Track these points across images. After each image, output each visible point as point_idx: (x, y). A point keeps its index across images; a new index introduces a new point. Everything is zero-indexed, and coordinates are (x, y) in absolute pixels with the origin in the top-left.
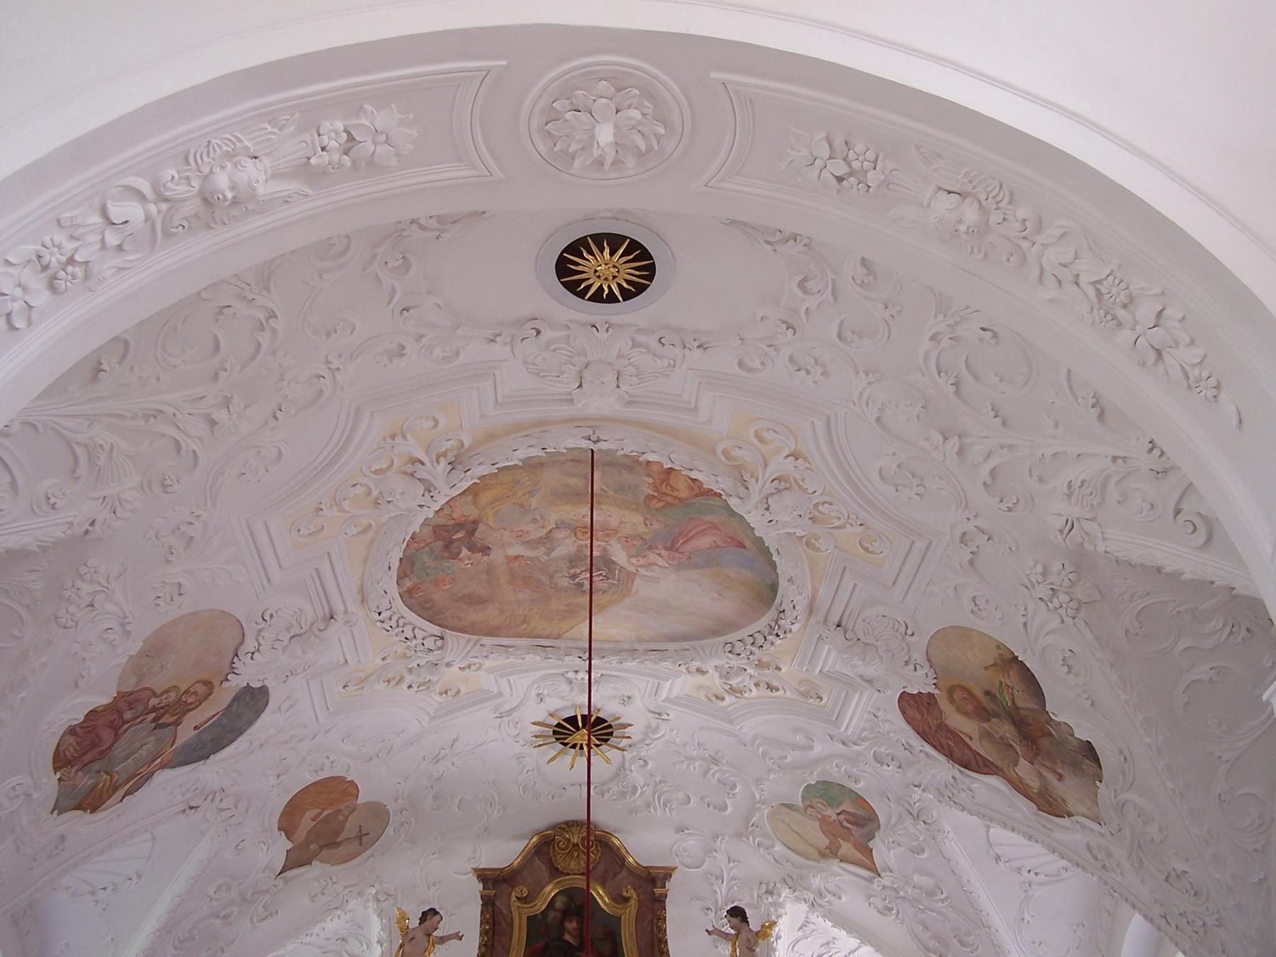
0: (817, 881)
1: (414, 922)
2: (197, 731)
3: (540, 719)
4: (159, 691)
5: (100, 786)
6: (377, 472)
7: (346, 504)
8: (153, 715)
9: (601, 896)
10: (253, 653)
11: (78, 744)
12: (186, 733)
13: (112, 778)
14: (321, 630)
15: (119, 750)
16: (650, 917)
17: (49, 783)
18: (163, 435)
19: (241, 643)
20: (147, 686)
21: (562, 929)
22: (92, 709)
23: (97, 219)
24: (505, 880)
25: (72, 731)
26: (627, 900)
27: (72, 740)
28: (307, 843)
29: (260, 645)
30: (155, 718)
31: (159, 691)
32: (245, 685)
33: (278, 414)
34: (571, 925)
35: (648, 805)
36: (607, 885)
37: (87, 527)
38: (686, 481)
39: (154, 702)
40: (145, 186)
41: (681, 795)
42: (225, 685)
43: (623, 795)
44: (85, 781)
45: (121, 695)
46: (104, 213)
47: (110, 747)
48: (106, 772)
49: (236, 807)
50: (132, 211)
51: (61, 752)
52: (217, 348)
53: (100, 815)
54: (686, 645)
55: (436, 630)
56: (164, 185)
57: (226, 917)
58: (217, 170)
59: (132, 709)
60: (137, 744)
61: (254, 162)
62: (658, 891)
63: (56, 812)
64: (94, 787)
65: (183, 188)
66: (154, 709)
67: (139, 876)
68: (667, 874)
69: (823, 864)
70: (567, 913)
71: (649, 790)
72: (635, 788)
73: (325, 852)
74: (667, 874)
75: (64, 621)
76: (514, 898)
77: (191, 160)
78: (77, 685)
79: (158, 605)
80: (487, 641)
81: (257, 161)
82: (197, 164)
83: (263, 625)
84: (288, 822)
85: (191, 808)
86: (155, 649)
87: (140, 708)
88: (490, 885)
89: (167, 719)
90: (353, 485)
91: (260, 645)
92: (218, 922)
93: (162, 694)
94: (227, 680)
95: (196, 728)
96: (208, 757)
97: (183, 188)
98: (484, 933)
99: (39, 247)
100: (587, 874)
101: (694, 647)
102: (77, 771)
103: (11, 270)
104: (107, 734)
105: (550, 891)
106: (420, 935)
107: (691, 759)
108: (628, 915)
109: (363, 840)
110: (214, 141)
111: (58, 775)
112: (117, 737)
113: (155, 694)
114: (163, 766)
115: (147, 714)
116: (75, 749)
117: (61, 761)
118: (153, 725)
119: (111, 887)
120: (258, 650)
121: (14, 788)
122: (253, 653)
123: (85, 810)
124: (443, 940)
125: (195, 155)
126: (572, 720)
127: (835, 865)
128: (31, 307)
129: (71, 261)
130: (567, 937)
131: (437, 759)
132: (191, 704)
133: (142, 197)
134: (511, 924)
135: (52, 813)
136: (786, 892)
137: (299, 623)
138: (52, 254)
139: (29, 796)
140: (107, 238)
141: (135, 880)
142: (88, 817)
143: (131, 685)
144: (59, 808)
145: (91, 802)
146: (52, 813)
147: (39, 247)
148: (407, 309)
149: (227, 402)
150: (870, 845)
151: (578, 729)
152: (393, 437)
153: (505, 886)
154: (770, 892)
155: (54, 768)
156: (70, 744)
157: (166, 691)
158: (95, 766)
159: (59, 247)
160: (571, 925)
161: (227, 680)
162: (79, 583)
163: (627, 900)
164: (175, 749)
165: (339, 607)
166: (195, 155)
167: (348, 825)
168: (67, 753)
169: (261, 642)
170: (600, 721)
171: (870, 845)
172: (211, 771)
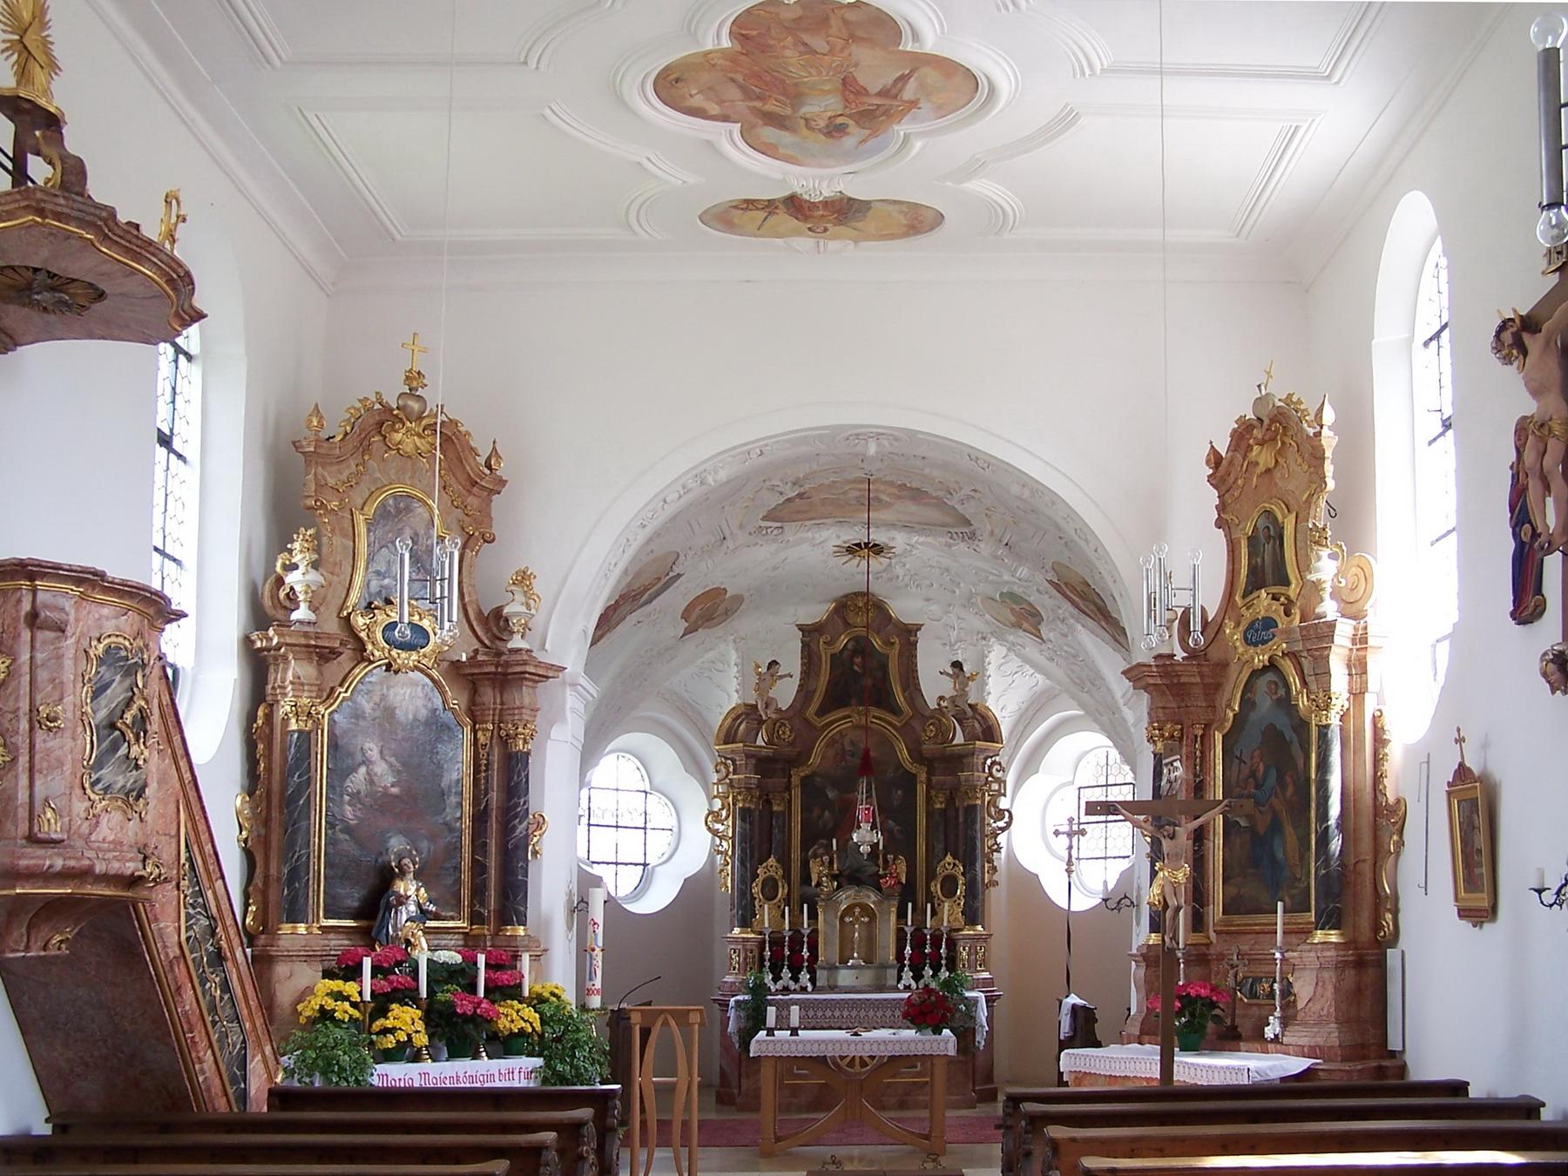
0: (1011, 638)
1: (763, 670)
9: (877, 643)
16: (907, 654)
21: (852, 663)
24: (816, 631)
26: (893, 644)
28: (696, 621)
34: (858, 660)
35: (907, 586)
41: (928, 582)
43: (890, 580)
54: (925, 527)
55: (779, 524)
62: (912, 639)
68: (919, 627)
69: (1013, 630)
70: (855, 652)
71: (907, 579)
72: (898, 577)
73: (706, 624)
74: (919, 627)
76: (821, 643)
80: (807, 523)
84: (686, 615)
88: (806, 634)
98: (803, 664)
100: (867, 626)
101: (930, 529)
105: (843, 640)
106: (768, 677)
107: (932, 567)
108: (894, 653)
109: (727, 613)
124: (781, 677)
126: (858, 545)
127: (1021, 633)
130: (856, 668)
131: (775, 568)
134: (820, 659)
136: (993, 640)
150: (1040, 627)
151: (862, 549)
153: (817, 634)
154: (984, 638)
160: (858, 660)
163: (893, 644)
165: (727, 534)
167: (720, 608)
170: (875, 545)
171: (1040, 627)
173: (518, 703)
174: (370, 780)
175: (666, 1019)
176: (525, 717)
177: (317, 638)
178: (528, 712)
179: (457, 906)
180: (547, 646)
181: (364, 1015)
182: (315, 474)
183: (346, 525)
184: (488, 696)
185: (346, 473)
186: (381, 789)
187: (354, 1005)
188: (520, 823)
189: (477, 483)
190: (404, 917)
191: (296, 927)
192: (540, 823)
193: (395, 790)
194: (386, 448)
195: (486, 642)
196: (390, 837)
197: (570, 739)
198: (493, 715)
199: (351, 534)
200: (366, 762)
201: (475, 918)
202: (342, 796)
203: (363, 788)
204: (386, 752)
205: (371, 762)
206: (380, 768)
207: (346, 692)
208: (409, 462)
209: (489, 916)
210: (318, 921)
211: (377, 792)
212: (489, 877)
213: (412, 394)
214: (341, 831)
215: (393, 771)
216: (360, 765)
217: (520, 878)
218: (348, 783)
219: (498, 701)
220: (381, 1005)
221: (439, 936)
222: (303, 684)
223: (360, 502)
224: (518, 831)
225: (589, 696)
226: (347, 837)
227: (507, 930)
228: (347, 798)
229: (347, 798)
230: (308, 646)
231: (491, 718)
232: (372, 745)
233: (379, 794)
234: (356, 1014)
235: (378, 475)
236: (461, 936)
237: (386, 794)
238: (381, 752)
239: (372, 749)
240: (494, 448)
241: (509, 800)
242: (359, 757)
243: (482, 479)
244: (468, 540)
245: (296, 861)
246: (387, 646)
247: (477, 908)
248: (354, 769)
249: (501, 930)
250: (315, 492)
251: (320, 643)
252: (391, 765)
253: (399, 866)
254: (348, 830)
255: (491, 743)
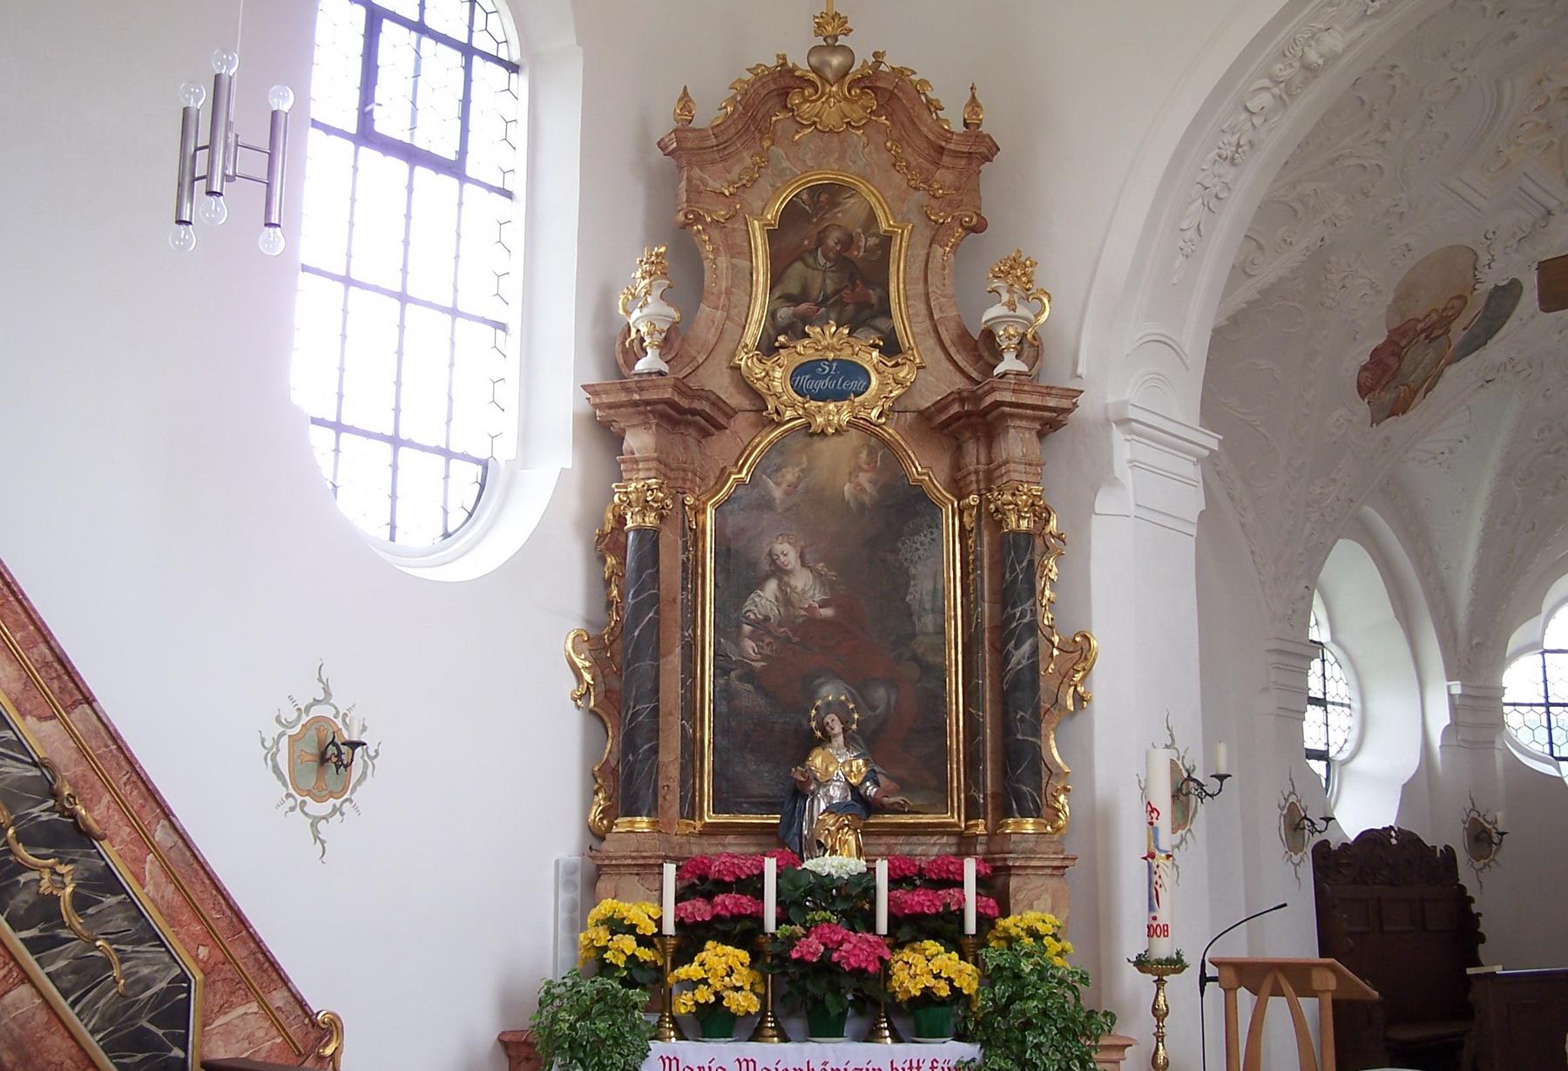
2: (1466, 331)
3: (1067, 870)
4: (1421, 318)
5: (1402, 395)
6: (1539, 108)
7: (1520, 140)
8: (1423, 335)
10: (1489, 264)
11: (1372, 374)
12: (1457, 333)
13: (1409, 387)
14: (1544, 227)
15: (1407, 366)
17: (1363, 408)
18: (1349, 166)
19: (1476, 260)
20: (1411, 317)
22: (1373, 348)
23: (1244, 115)
25: (1364, 368)
27: (1366, 374)
29: (1493, 256)
30: (1426, 336)
31: (1421, 318)
32: (1493, 286)
33: (1430, 114)
36: (686, 1035)
37: (1319, 243)
38: (1274, 668)
39: (1420, 326)
40: (1266, 82)
42: (1476, 293)
44: (1388, 397)
45: (1394, 334)
46: (1246, 109)
47: (1398, 369)
48: (1403, 385)
49: (1531, 366)
50: (1265, 99)
51: (1363, 385)
52: (1362, 102)
53: (1410, 413)
56: (1277, 76)
57: (1557, 451)
58: (1306, 49)
59: (1405, 337)
60: (1420, 358)
61: (1329, 33)
63: (1374, 425)
64: (1398, 396)
65: (1289, 71)
66: (1423, 331)
67: (1468, 438)
75: (1328, 304)
77: (1287, 53)
78: (1355, 339)
79: (1395, 264)
81: (1331, 31)
82: (1290, 53)
83: (1489, 242)
85: (1488, 382)
86: (1406, 292)
87: (1411, 334)
89: (1436, 333)
90: (1521, 126)
91: (1493, 256)
92: (1550, 457)
93: (1425, 318)
94: (1475, 289)
95: (1465, 329)
96: (1486, 343)
97: (1289, 71)
99: (1217, 151)
102: (1379, 393)
103: (1207, 172)
104: (1392, 361)
110: (1298, 36)
111: (1366, 401)
112: (1401, 359)
113: (1419, 321)
114: (1449, 363)
115: (1418, 335)
116: (1372, 379)
117: (1363, 390)
118: (1427, 341)
119: (1448, 451)
120: (1493, 260)
121: (1337, 420)
122: (1489, 264)
123: (1397, 415)
125: (1289, 50)
128: (1226, 183)
129: (1238, 145)
132: (1452, 316)
133: (1267, 89)
135: (1371, 426)
137: (1520, 229)
138: (1226, 150)
139: (1350, 421)
140: (1255, 122)
141: (1465, 442)
142: (1402, 418)
143: (1396, 323)
144: (1376, 421)
145: (1400, 408)
146: (1371, 426)
147: (1217, 151)
148: (1502, 13)
149: (1387, 127)
152: (1540, 82)
155: (1361, 397)
156: (1367, 377)
157: (1428, 316)
158: (1393, 384)
159: (1229, 144)
161: (1475, 289)
162: (1329, 276)
164: (1454, 349)
166: (1289, 50)
168: (1368, 384)
169: (1493, 253)
172: (1496, 350)
173: (1004, 456)
174: (785, 599)
175: (1276, 979)
176: (1015, 476)
177: (641, 389)
178: (1021, 468)
179: (943, 787)
180: (1080, 371)
181: (664, 956)
182: (689, 180)
183: (738, 241)
184: (974, 455)
185: (737, 169)
186: (803, 613)
187: (643, 941)
188: (1017, 647)
189: (942, 148)
190: (823, 806)
191: (632, 823)
192: (1080, 652)
193: (827, 612)
194: (796, 126)
195: (974, 375)
196: (822, 684)
197: (1132, 510)
198: (978, 482)
199: (747, 250)
200: (779, 572)
201: (973, 811)
202: (739, 627)
203: (774, 612)
204: (808, 557)
205: (788, 573)
206: (802, 581)
207: (740, 471)
208: (836, 139)
209: (985, 805)
210: (701, 817)
211: (796, 617)
212: (984, 741)
213: (832, 47)
214: (740, 678)
215: (823, 584)
216: (767, 577)
217: (1019, 737)
218: (748, 605)
219: (983, 459)
220: (690, 939)
221: (914, 839)
222: (636, 461)
223: (758, 204)
224: (1014, 660)
225: (1200, 449)
226: (749, 687)
227: (1007, 825)
228: (747, 628)
229: (747, 628)
230: (635, 404)
231: (974, 486)
232: (786, 547)
233: (801, 620)
234: (645, 954)
235: (786, 164)
236: (953, 840)
237: (812, 621)
238: (802, 556)
239: (787, 553)
240: (973, 97)
241: (1004, 608)
242: (765, 566)
243: (948, 141)
244: (938, 230)
245: (631, 721)
246: (800, 398)
247: (972, 793)
248: (759, 584)
249: (1002, 826)
250: (688, 201)
251: (647, 396)
252: (818, 575)
253: (823, 727)
254: (750, 675)
255: (979, 528)
